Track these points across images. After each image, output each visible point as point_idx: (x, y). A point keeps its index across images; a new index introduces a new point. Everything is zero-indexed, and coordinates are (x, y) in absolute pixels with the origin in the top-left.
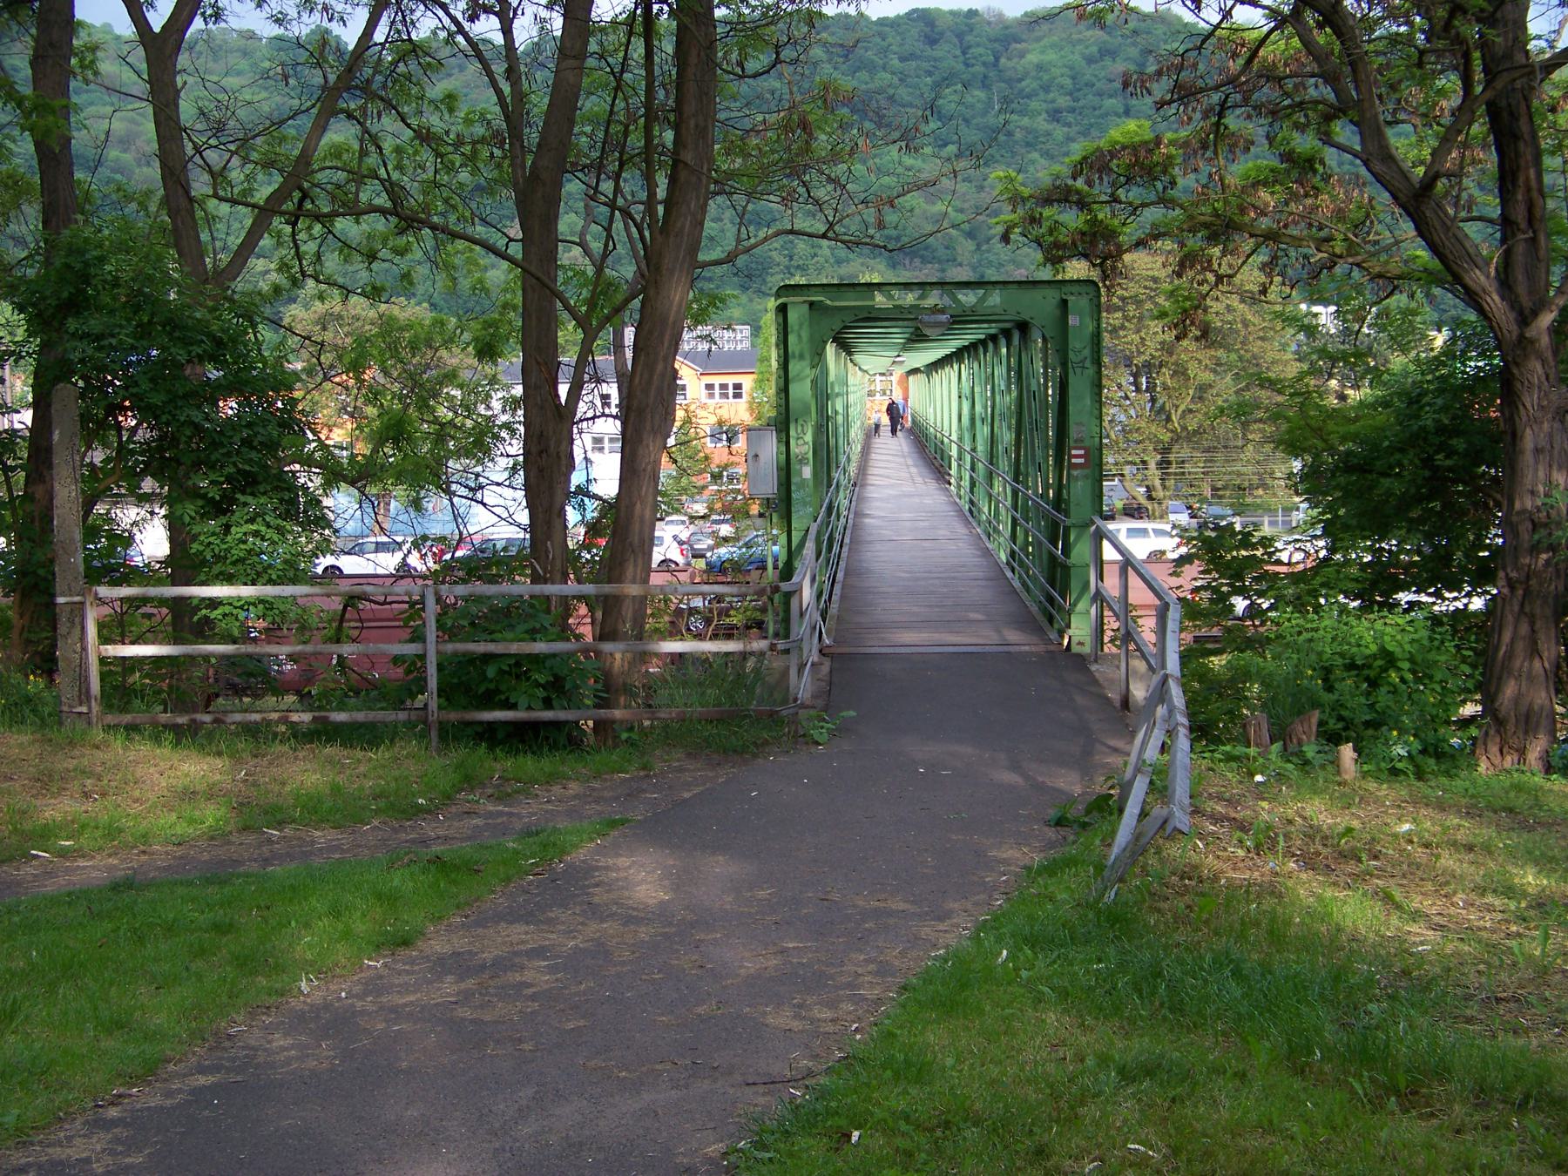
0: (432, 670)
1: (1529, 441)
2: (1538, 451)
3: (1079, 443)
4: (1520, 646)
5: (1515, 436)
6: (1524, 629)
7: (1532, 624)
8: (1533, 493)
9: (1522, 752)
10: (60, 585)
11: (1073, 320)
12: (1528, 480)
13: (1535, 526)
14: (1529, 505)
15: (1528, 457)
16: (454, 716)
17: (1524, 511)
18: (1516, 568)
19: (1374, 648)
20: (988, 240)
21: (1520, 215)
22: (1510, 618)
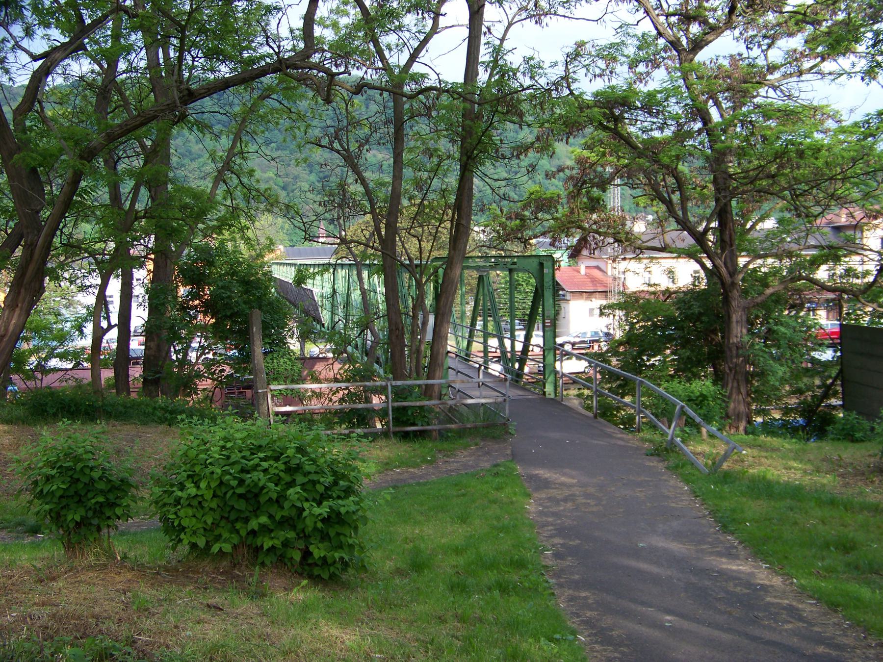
0: (390, 413)
1: (734, 318)
2: (737, 322)
3: (548, 317)
4: (734, 390)
5: (729, 317)
6: (735, 385)
7: (738, 383)
8: (736, 337)
9: (737, 428)
10: (259, 385)
11: (546, 271)
12: (734, 332)
13: (738, 348)
14: (735, 341)
15: (734, 324)
16: (397, 429)
17: (733, 343)
18: (732, 363)
19: (698, 394)
20: (293, 191)
21: (727, 238)
22: (730, 381)
